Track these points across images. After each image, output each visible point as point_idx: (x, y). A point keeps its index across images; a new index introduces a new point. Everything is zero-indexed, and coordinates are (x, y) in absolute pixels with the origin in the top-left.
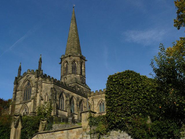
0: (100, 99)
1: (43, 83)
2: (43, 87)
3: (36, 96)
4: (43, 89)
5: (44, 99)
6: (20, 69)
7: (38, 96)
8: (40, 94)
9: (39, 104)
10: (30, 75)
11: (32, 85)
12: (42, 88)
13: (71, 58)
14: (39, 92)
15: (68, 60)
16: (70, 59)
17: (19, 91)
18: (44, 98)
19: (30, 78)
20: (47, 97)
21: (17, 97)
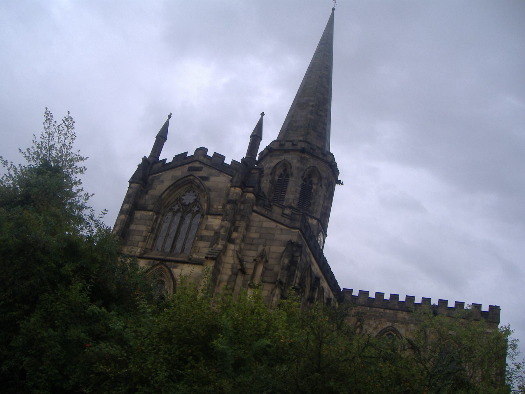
0: (389, 324)
1: (254, 214)
2: (253, 229)
3: (224, 251)
4: (254, 235)
5: (250, 272)
6: (162, 138)
7: (230, 253)
8: (237, 248)
9: (228, 282)
10: (205, 169)
11: (210, 206)
12: (248, 228)
13: (304, 158)
14: (238, 241)
15: (295, 161)
16: (302, 160)
17: (144, 209)
18: (249, 267)
19: (206, 179)
20: (265, 269)
21: (133, 227)
